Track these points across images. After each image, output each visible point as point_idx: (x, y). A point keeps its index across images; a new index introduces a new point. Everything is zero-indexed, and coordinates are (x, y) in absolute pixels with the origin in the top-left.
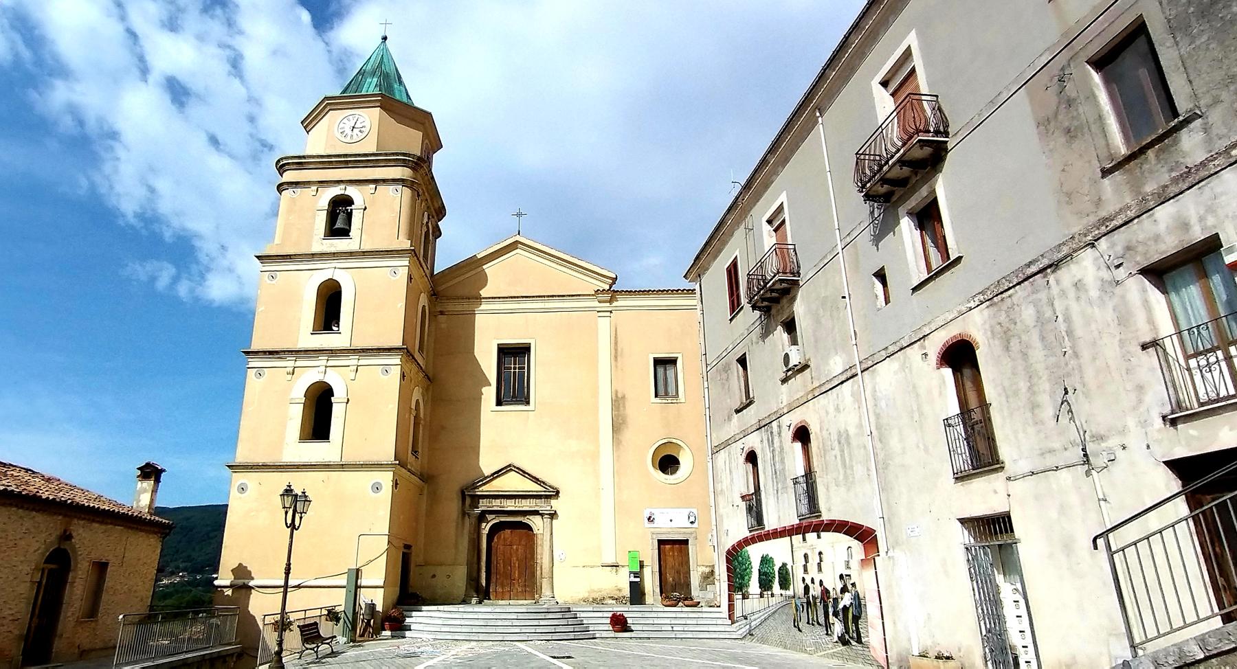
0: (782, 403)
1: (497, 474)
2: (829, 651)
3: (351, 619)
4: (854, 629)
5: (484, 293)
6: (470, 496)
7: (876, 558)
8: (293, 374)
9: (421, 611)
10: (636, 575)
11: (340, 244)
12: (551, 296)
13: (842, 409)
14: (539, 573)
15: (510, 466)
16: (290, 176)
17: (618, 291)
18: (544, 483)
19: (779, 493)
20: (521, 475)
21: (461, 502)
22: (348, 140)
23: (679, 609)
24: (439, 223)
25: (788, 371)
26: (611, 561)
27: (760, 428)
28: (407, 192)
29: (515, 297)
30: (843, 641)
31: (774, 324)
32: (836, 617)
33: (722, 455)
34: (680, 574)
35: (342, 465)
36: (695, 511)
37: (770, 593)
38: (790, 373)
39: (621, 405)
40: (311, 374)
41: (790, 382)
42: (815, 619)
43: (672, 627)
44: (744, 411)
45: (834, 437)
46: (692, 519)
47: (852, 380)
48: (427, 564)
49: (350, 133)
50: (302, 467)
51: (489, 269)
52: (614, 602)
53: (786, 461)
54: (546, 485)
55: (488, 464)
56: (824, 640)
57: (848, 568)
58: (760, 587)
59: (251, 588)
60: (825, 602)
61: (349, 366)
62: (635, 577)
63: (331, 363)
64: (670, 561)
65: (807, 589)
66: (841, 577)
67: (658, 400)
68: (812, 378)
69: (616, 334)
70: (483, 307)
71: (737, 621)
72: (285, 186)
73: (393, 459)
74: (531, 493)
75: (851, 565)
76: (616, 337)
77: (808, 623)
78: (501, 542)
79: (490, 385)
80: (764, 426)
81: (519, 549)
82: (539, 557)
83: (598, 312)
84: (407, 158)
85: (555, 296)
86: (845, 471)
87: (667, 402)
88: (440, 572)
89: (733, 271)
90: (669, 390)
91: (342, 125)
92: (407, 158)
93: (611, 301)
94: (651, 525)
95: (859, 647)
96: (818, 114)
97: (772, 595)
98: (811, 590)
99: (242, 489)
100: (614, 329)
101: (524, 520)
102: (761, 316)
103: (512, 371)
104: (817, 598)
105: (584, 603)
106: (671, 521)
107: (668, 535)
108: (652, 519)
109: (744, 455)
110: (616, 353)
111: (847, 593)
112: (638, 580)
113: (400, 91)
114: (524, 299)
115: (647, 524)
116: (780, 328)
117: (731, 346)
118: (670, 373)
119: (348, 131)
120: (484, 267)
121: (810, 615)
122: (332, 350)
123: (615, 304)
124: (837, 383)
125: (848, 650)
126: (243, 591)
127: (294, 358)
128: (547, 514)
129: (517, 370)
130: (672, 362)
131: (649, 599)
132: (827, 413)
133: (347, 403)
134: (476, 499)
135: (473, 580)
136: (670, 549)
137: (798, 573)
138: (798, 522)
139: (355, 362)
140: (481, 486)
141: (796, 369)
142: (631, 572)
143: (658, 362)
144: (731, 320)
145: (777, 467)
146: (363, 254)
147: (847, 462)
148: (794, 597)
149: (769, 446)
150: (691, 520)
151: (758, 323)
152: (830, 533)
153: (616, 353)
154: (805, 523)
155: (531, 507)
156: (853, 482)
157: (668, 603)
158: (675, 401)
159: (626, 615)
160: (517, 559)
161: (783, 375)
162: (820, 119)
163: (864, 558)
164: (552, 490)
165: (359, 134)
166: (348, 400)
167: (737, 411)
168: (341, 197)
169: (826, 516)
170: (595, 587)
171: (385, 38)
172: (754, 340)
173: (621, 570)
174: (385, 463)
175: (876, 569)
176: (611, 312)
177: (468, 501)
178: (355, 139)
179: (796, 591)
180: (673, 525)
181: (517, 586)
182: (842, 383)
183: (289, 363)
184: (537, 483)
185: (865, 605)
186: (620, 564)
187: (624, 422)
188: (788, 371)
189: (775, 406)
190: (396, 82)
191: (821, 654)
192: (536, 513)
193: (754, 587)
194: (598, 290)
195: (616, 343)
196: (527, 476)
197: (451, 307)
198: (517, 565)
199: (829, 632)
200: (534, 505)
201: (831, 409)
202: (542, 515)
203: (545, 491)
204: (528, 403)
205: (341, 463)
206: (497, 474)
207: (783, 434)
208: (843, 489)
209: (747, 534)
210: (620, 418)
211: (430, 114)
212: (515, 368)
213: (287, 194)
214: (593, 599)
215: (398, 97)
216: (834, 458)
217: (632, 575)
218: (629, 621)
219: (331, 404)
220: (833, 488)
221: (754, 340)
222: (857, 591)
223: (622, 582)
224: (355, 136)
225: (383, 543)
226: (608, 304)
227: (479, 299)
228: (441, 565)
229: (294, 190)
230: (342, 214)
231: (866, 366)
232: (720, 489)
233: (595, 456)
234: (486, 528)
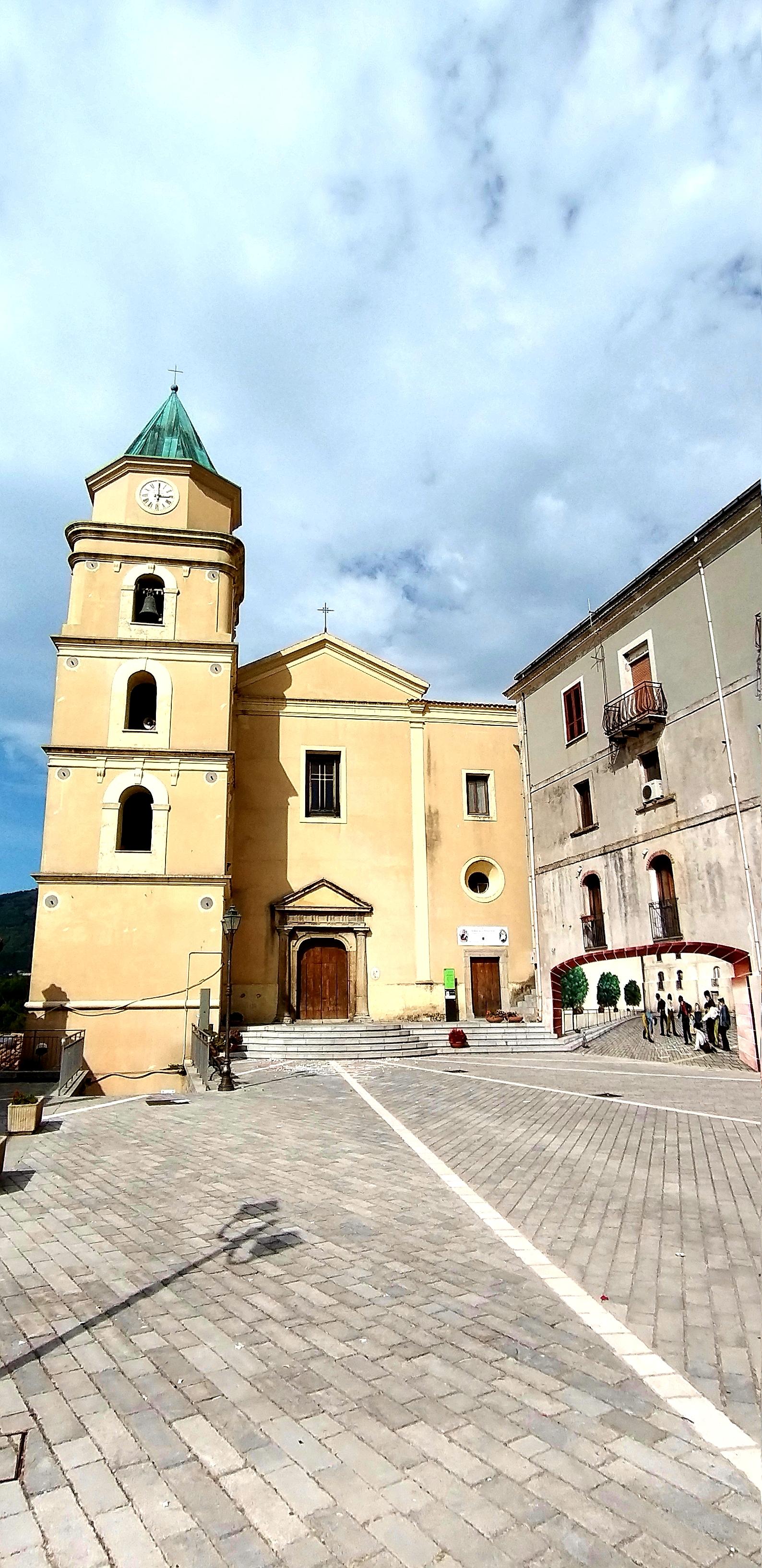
0: (636, 832)
2: (689, 1059)
4: (721, 1038)
5: (288, 694)
6: (279, 911)
7: (750, 976)
9: (247, 1031)
11: (150, 632)
12: (362, 702)
13: (713, 843)
14: (352, 991)
15: (322, 880)
17: (431, 702)
18: (358, 899)
19: (628, 916)
20: (335, 891)
22: (152, 510)
23: (505, 1025)
25: (647, 803)
26: (426, 979)
27: (605, 853)
28: (224, 578)
29: (323, 701)
30: (705, 1048)
31: (629, 757)
32: (698, 1028)
33: (549, 878)
35: (168, 878)
36: (506, 929)
37: (612, 1008)
38: (651, 804)
39: (434, 821)
41: (647, 813)
42: (671, 1030)
44: (584, 836)
45: (703, 867)
46: (503, 937)
47: (727, 818)
49: (154, 502)
50: (123, 879)
51: (293, 667)
52: (429, 1019)
53: (638, 886)
54: (360, 901)
55: (296, 879)
56: (682, 1049)
57: (715, 984)
58: (598, 1003)
60: (684, 1015)
61: (169, 770)
62: (450, 994)
63: (147, 765)
64: (481, 978)
65: (662, 1004)
66: (707, 993)
67: (470, 817)
68: (677, 812)
69: (429, 747)
70: (288, 709)
71: (566, 1035)
72: (82, 558)
73: (224, 873)
74: (345, 910)
75: (719, 982)
76: (429, 750)
77: (663, 1034)
78: (311, 959)
79: (297, 795)
80: (611, 852)
81: (329, 967)
82: (352, 975)
83: (411, 722)
84: (225, 540)
85: (366, 702)
86: (715, 900)
87: (479, 819)
88: (251, 990)
89: (573, 699)
91: (144, 492)
92: (225, 540)
93: (424, 712)
94: (464, 943)
95: (726, 1054)
96: (700, 565)
97: (616, 1010)
98: (666, 1005)
99: (52, 902)
101: (337, 937)
102: (611, 747)
103: (320, 779)
104: (675, 1012)
106: (483, 939)
107: (479, 953)
109: (581, 878)
111: (712, 1008)
112: (453, 997)
113: (202, 456)
114: (334, 703)
115: (461, 943)
116: (637, 761)
117: (567, 771)
118: (481, 790)
119: (153, 500)
120: (288, 665)
121: (665, 1027)
122: (149, 751)
123: (427, 715)
124: (709, 820)
125: (713, 1057)
126: (60, 1014)
127: (105, 758)
129: (320, 775)
130: (484, 778)
131: (462, 1015)
132: (695, 845)
133: (169, 811)
134: (285, 915)
135: (284, 999)
136: (481, 967)
137: (652, 989)
138: (652, 943)
139: (176, 766)
140: (291, 901)
141: (658, 802)
144: (568, 746)
145: (627, 891)
146: (180, 645)
147: (718, 890)
148: (645, 1011)
149: (616, 871)
150: (502, 938)
151: (607, 752)
152: (693, 954)
153: (429, 767)
154: (660, 944)
155: (344, 924)
156: (724, 910)
157: (495, 1019)
159: (465, 1031)
160: (329, 977)
161: (640, 806)
162: (702, 570)
163: (734, 977)
164: (366, 906)
165: (166, 505)
166: (170, 808)
167: (573, 835)
168: (149, 576)
169: (687, 939)
171: (175, 389)
172: (601, 768)
173: (435, 987)
174: (216, 877)
175: (749, 986)
177: (277, 917)
178: (162, 510)
179: (648, 1005)
180: (485, 943)
181: (328, 1005)
182: (715, 820)
183: (100, 763)
184: (350, 899)
185: (735, 1018)
187: (438, 838)
188: (647, 803)
189: (627, 834)
191: (681, 1061)
193: (591, 1001)
194: (412, 700)
195: (429, 756)
196: (340, 891)
199: (689, 1042)
201: (701, 844)
203: (359, 908)
204: (338, 815)
207: (636, 861)
208: (711, 916)
209: (583, 953)
210: (434, 834)
211: (240, 489)
212: (322, 777)
213: (81, 567)
215: (201, 463)
216: (701, 887)
217: (448, 992)
218: (468, 1037)
220: (699, 914)
221: (601, 768)
222: (725, 1006)
223: (438, 999)
224: (161, 507)
226: (421, 715)
228: (251, 984)
229: (92, 562)
231: (746, 807)
232: (545, 909)
233: (409, 872)
234: (296, 945)
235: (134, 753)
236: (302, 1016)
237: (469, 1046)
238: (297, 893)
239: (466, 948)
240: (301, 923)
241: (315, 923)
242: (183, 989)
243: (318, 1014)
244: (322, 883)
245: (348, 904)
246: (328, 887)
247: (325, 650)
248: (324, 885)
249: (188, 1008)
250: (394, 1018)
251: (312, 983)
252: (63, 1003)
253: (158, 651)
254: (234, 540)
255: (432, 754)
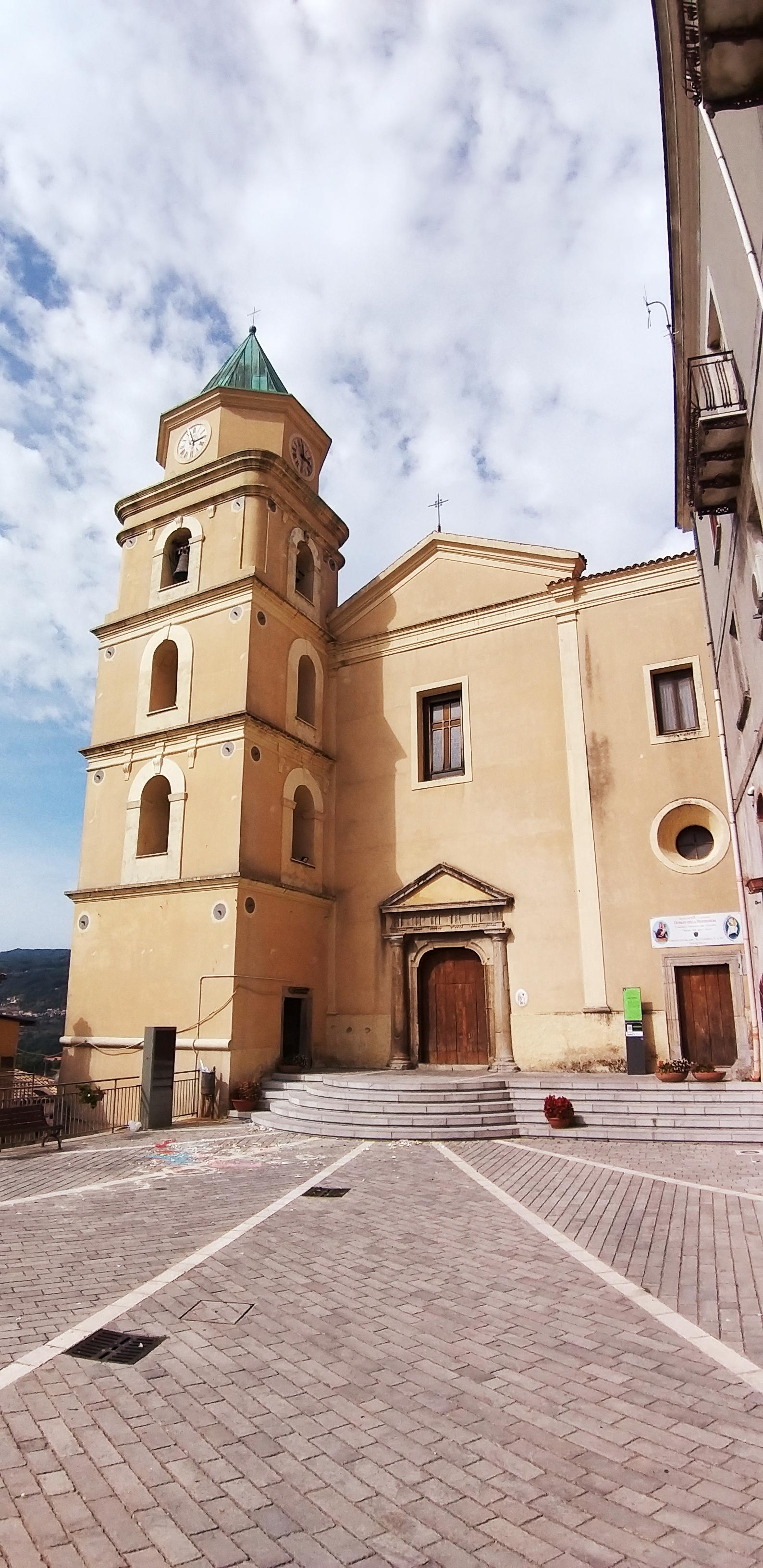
1: (424, 880)
3: (149, 1099)
8: (130, 771)
10: (636, 1026)
11: (180, 592)
15: (439, 866)
16: (132, 522)
18: (488, 887)
21: (380, 926)
22: (189, 458)
24: (341, 550)
28: (253, 503)
34: (718, 1022)
39: (602, 754)
40: (145, 774)
43: (654, 1121)
46: (733, 929)
48: (340, 1012)
52: (606, 1068)
54: (493, 891)
59: (91, 1047)
62: (634, 1029)
67: (663, 739)
74: (471, 905)
76: (587, 650)
83: (557, 616)
90: (686, 719)
93: (575, 595)
100: (584, 637)
101: (469, 946)
105: (559, 1070)
106: (696, 934)
108: (663, 933)
110: (589, 674)
112: (640, 1034)
115: (656, 944)
120: (392, 591)
123: (583, 599)
128: (496, 935)
130: (684, 673)
133: (186, 800)
139: (192, 744)
140: (403, 899)
142: (628, 1023)
143: (658, 677)
153: (589, 674)
155: (473, 925)
158: (692, 736)
160: (465, 1004)
164: (500, 898)
166: (186, 795)
170: (576, 1044)
174: (225, 876)
176: (577, 612)
177: (389, 923)
180: (702, 941)
181: (465, 1043)
183: (125, 758)
184: (479, 889)
186: (614, 1008)
187: (608, 780)
190: (256, 372)
192: (480, 934)
194: (552, 583)
195: (588, 660)
196: (464, 879)
197: (355, 653)
198: (464, 1012)
200: (479, 922)
202: (490, 936)
203: (490, 901)
205: (180, 881)
206: (424, 880)
214: (573, 1064)
218: (576, 1107)
219: (168, 804)
224: (194, 454)
225: (228, 988)
226: (571, 602)
227: (383, 635)
228: (360, 1014)
229: (131, 540)
230: (183, 554)
233: (565, 840)
234: (415, 960)
235: (153, 738)
236: (432, 1059)
237: (585, 1125)
238: (408, 887)
239: (665, 952)
240: (416, 929)
241: (436, 928)
242: (192, 1025)
243: (453, 1056)
244: (438, 871)
245: (474, 896)
246: (450, 875)
247: (438, 555)
248: (442, 872)
249: (196, 1049)
250: (552, 1066)
251: (443, 1012)
252: (87, 1038)
253: (181, 613)
254: (260, 454)
255: (593, 656)
